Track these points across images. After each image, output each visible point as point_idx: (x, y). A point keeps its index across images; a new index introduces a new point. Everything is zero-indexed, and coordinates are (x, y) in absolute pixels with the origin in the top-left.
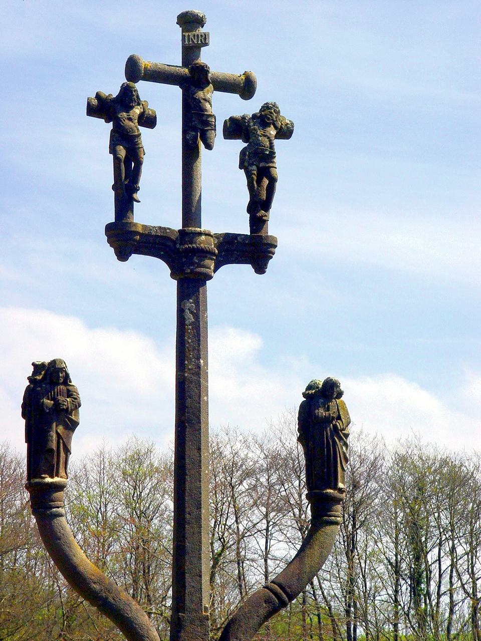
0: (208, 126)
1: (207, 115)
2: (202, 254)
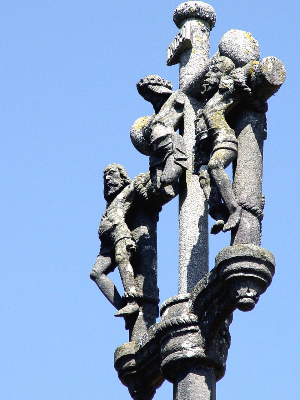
0: (166, 153)
1: (154, 142)
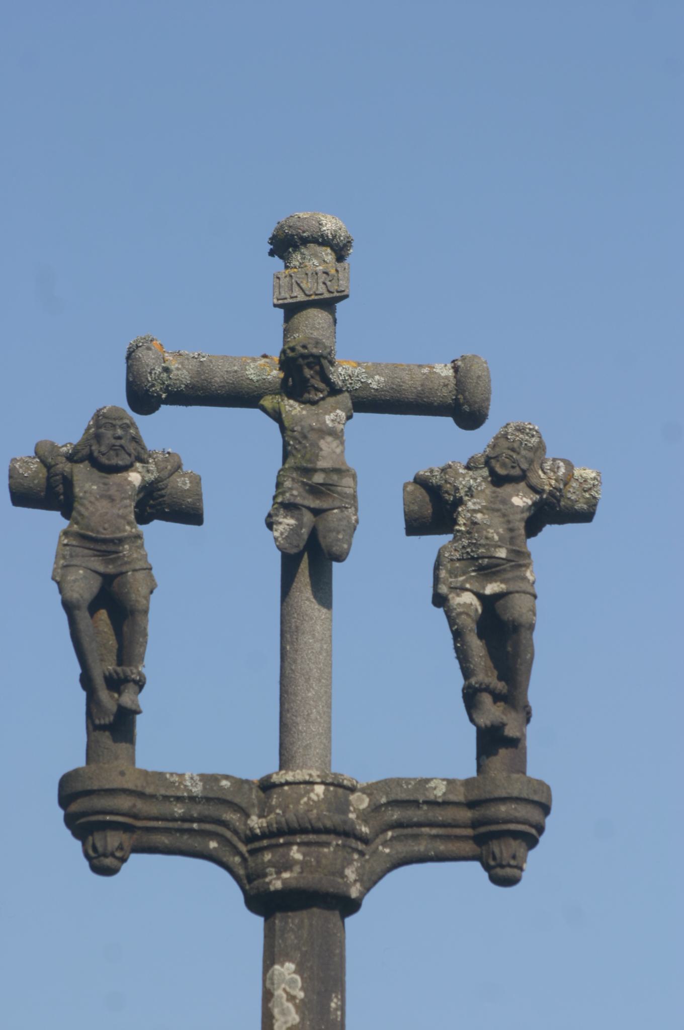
2: (312, 837)
